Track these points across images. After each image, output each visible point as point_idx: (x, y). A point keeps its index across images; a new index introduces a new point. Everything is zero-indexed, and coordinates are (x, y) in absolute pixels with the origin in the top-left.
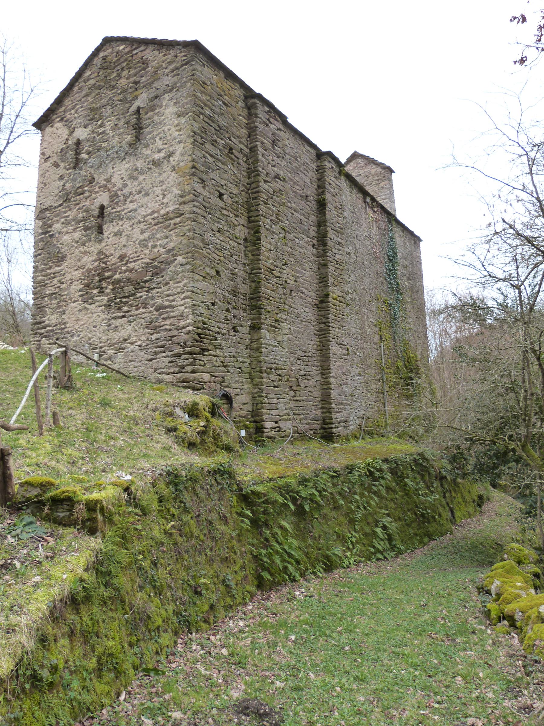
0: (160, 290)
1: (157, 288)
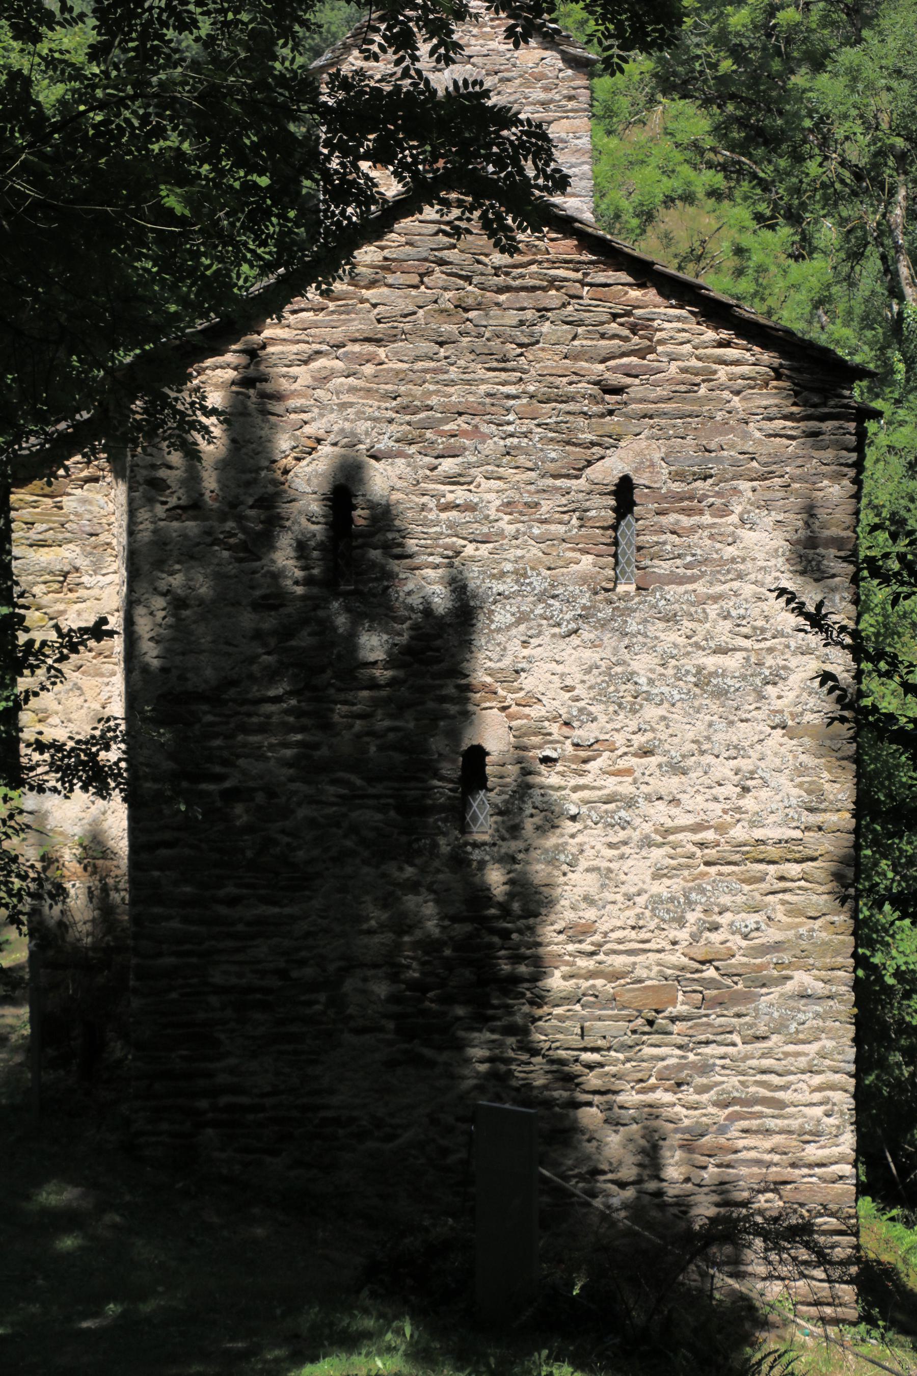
0: (730, 1049)
1: (720, 1044)
